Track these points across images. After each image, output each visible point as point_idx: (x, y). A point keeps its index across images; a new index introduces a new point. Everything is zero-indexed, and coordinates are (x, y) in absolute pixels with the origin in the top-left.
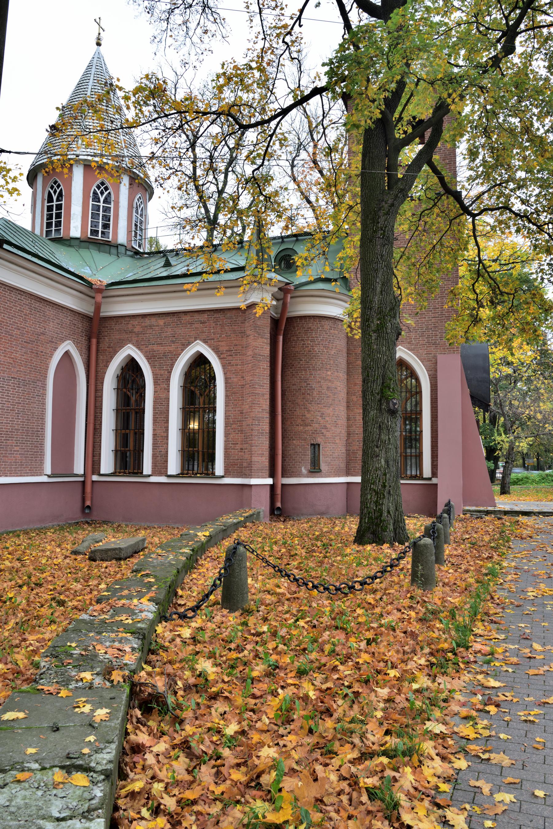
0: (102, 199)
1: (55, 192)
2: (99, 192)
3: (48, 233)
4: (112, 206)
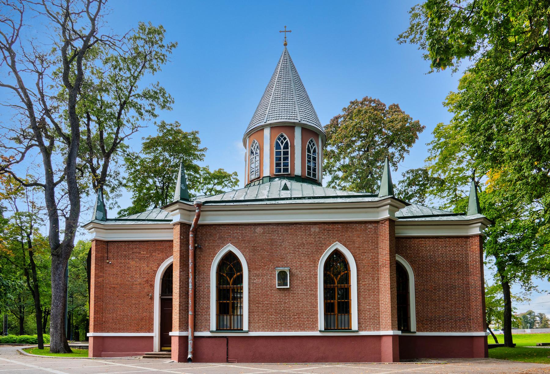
0: (282, 147)
1: (282, 143)
2: (280, 142)
3: (279, 171)
4: (289, 150)
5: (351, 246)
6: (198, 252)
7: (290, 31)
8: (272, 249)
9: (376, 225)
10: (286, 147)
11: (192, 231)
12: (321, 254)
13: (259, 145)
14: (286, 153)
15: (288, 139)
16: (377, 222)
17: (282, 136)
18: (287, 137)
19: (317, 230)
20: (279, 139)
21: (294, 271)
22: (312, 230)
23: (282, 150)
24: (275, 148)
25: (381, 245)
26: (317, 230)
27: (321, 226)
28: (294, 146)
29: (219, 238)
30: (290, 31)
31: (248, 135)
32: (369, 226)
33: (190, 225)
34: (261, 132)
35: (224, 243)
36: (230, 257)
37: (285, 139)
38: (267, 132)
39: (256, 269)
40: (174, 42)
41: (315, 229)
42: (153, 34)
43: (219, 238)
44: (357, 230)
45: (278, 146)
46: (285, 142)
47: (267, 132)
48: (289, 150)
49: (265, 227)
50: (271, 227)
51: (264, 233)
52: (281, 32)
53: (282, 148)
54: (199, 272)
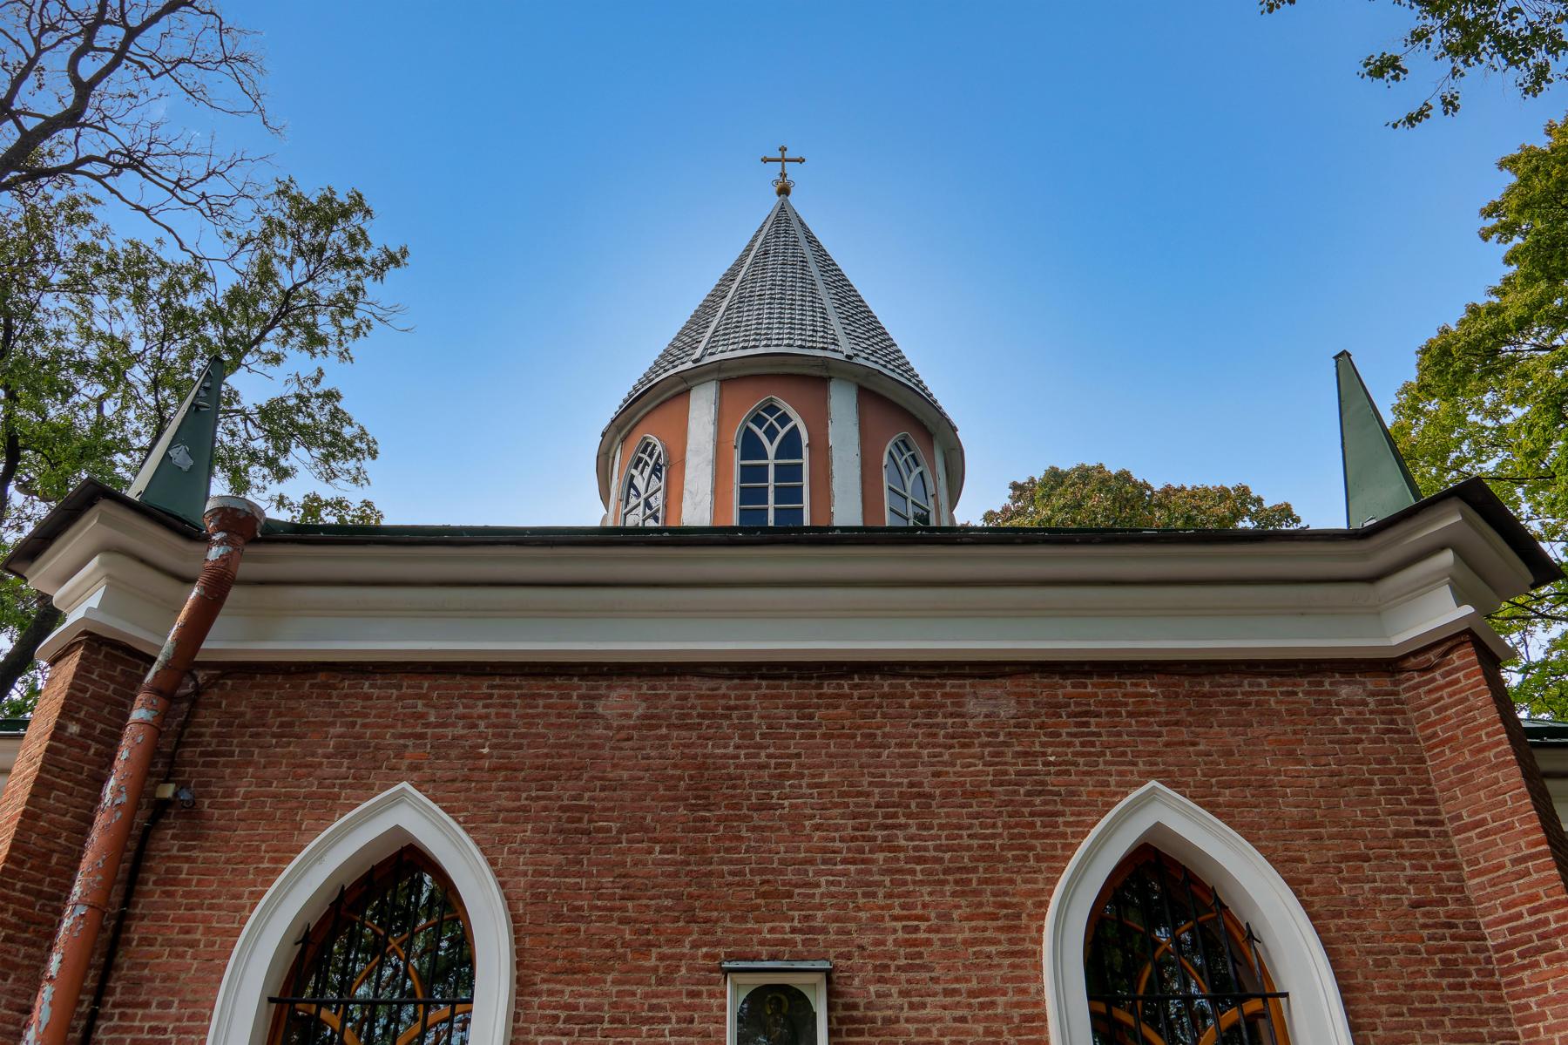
0: (771, 450)
2: (760, 433)
4: (805, 461)
5: (1252, 815)
6: (168, 841)
7: (802, 161)
8: (700, 826)
9: (1386, 684)
10: (790, 445)
11: (156, 690)
12: (1055, 863)
13: (666, 449)
14: (789, 473)
15: (797, 420)
16: (1387, 666)
17: (771, 409)
18: (792, 413)
19: (1007, 709)
20: (759, 420)
21: (864, 989)
22: (971, 706)
23: (771, 462)
24: (737, 454)
25: (1457, 804)
26: (1007, 709)
27: (1026, 684)
28: (828, 448)
29: (342, 751)
30: (802, 161)
31: (619, 431)
32: (1344, 691)
33: (153, 660)
34: (674, 408)
35: (366, 771)
36: (399, 883)
37: (784, 420)
38: (702, 410)
39: (573, 969)
40: (394, 249)
41: (983, 704)
42: (321, 220)
43: (342, 751)
44: (1268, 715)
45: (751, 446)
46: (782, 432)
47: (702, 410)
48: (805, 461)
49: (663, 687)
50: (704, 685)
51: (649, 721)
52: (765, 160)
53: (771, 450)
54: (136, 984)
